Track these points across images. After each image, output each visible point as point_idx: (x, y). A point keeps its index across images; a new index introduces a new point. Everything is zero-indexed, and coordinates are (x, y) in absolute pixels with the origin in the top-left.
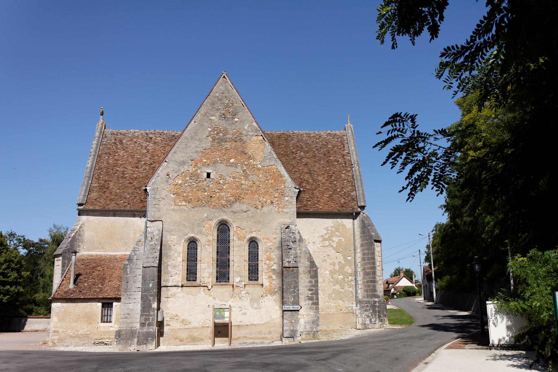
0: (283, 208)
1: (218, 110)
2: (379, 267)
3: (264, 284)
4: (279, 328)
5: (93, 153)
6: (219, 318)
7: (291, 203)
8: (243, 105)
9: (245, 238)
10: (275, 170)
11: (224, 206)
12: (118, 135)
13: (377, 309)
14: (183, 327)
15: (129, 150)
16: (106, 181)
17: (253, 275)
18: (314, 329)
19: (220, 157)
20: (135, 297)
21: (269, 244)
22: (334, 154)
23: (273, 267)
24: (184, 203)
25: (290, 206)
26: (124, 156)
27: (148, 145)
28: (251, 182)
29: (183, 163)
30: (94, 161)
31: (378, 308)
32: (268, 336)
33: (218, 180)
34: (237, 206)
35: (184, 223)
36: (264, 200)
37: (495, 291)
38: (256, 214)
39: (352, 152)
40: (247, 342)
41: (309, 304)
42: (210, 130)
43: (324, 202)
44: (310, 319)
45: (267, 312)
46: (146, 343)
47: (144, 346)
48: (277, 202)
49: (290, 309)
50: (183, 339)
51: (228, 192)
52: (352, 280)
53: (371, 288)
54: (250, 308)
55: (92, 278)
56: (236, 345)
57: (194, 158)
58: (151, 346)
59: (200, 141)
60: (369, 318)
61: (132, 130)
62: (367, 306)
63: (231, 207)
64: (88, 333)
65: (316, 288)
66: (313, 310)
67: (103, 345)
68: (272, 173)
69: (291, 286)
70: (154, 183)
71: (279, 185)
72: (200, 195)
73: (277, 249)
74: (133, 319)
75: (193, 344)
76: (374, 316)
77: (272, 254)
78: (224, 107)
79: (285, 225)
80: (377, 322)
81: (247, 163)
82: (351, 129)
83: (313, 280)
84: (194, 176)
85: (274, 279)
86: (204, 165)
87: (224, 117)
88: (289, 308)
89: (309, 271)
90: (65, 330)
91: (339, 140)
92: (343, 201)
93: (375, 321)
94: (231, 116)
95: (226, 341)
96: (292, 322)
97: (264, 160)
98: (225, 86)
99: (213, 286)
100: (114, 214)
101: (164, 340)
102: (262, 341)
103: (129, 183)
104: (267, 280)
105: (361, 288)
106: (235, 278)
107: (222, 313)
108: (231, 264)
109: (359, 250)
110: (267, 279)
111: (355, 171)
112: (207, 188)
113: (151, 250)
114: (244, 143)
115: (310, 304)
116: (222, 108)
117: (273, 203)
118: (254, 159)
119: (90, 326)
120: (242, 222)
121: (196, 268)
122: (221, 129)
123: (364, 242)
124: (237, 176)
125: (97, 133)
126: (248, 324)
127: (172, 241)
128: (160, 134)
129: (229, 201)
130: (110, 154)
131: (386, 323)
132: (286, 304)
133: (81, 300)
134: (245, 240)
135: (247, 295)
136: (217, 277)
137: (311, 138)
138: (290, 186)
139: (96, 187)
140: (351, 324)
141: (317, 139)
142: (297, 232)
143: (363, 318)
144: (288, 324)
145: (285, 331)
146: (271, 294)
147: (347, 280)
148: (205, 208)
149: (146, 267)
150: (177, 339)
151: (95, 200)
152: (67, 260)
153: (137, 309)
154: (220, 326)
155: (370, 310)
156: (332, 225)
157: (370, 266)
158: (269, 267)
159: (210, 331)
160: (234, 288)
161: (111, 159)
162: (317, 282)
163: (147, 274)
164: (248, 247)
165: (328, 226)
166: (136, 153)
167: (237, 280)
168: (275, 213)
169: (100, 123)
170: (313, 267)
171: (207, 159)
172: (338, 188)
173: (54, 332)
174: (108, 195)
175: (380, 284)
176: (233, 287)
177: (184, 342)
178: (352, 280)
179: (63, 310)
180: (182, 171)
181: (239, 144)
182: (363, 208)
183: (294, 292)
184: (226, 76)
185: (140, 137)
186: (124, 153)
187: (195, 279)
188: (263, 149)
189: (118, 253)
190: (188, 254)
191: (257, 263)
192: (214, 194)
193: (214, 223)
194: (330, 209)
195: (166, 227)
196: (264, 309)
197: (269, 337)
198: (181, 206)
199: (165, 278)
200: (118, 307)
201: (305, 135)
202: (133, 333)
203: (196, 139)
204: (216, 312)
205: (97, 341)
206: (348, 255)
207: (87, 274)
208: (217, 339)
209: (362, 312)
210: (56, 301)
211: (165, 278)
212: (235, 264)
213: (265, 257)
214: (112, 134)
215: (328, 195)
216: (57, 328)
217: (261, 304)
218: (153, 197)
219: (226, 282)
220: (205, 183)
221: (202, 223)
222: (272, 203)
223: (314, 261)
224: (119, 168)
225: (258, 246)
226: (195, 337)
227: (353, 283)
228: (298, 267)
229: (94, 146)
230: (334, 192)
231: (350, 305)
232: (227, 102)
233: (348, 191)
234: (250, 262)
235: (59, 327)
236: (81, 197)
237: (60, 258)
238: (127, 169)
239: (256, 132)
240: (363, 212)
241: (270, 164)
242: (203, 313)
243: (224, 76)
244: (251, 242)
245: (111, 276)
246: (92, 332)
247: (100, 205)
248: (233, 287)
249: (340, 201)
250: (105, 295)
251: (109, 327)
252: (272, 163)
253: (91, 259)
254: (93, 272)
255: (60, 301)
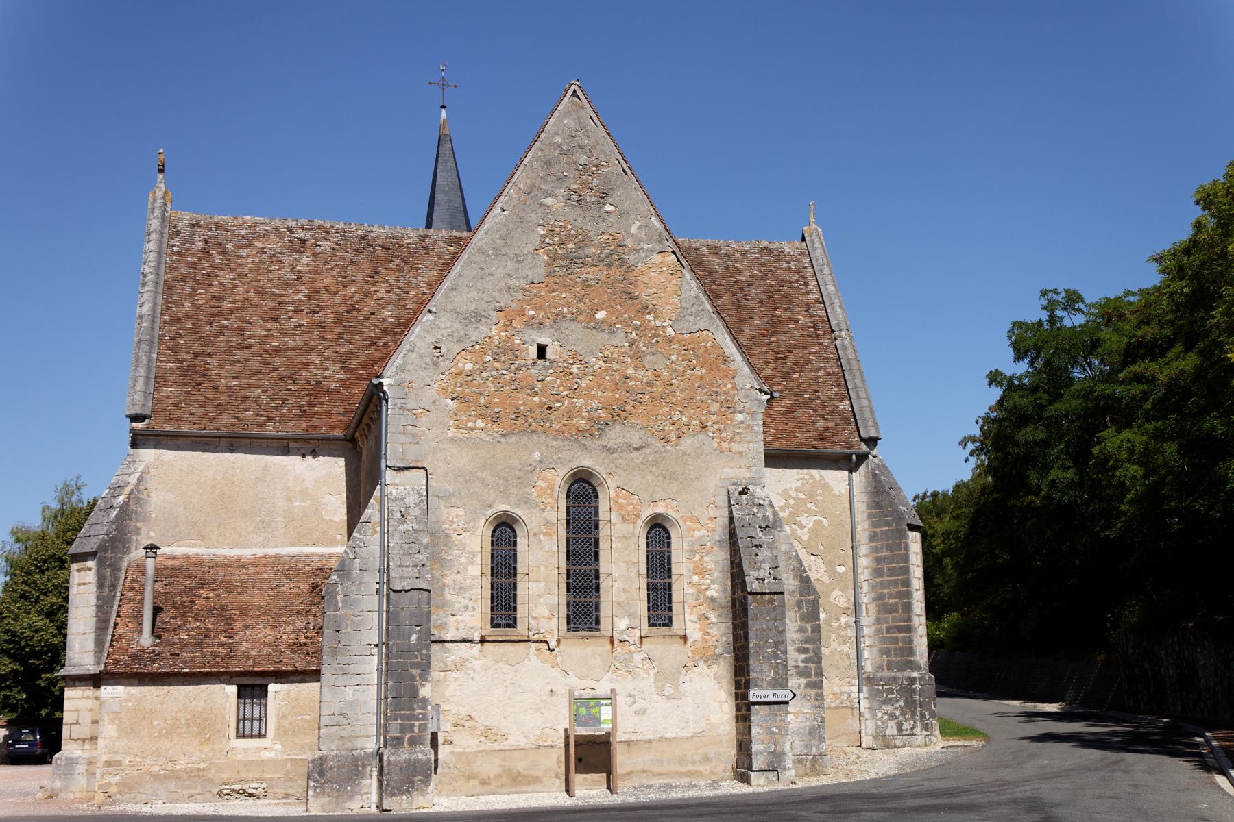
0: (732, 441)
1: (562, 180)
2: (919, 592)
3: (688, 635)
4: (727, 747)
5: (150, 277)
6: (585, 724)
7: (750, 428)
8: (624, 171)
9: (638, 516)
10: (709, 344)
11: (582, 433)
12: (210, 230)
13: (917, 697)
14: (487, 748)
15: (246, 271)
16: (196, 355)
17: (659, 612)
18: (814, 749)
19: (569, 304)
20: (360, 668)
21: (698, 534)
22: (785, 303)
23: (709, 593)
24: (480, 423)
25: (748, 437)
26: (235, 287)
27: (298, 260)
28: (649, 373)
29: (475, 318)
30: (156, 297)
31: (920, 696)
32: (702, 769)
33: (565, 365)
34: (616, 435)
35: (484, 476)
36: (684, 419)
37: (1163, 652)
38: (664, 455)
39: (830, 299)
40: (651, 783)
41: (800, 686)
42: (542, 232)
43: (775, 427)
44: (802, 724)
45: (698, 707)
46: (408, 791)
47: (404, 797)
48: (716, 426)
49: (766, 699)
50: (489, 778)
51: (592, 397)
52: (849, 626)
53: (900, 644)
54: (655, 697)
55: (195, 619)
56: (626, 794)
57: (503, 305)
58: (420, 798)
59: (519, 261)
60: (896, 721)
61: (249, 218)
62: (890, 691)
63: (600, 435)
64: (202, 766)
65: (816, 646)
66: (808, 701)
67: (242, 797)
68: (702, 351)
69: (767, 642)
70: (401, 368)
71: (720, 382)
72: (521, 402)
73: (720, 547)
74: (357, 729)
75: (514, 790)
76: (908, 716)
77: (706, 559)
78: (577, 173)
79: (738, 485)
80: (918, 730)
81: (638, 323)
82: (819, 238)
83: (809, 627)
84: (506, 352)
85: (713, 623)
86: (530, 323)
87: (576, 199)
88: (765, 696)
89: (797, 602)
90: (139, 760)
91: (792, 265)
92: (821, 423)
93: (912, 729)
94: (594, 199)
95: (599, 781)
96: (773, 733)
97: (680, 318)
98: (579, 118)
99: (563, 641)
100: (232, 445)
101: (440, 782)
102: (688, 780)
103: (261, 363)
104: (697, 626)
105: (870, 646)
106: (615, 619)
107: (594, 710)
108: (604, 583)
109: (863, 550)
110: (695, 622)
111: (844, 348)
112: (539, 386)
113: (406, 546)
114: (630, 269)
115: (802, 686)
116: (572, 176)
117: (706, 427)
118: (657, 314)
119: (206, 749)
120: (630, 476)
121: (515, 595)
122: (570, 230)
123: (878, 530)
124: (615, 356)
125: (155, 221)
126: (651, 737)
127: (452, 521)
128: (327, 232)
129: (597, 421)
130: (198, 282)
131: (935, 733)
132: (755, 686)
133: (181, 679)
134: (640, 522)
135: (647, 664)
136: (568, 616)
137: (722, 259)
138: (748, 386)
139: (172, 370)
140: (847, 735)
141: (736, 261)
142: (767, 503)
143: (878, 720)
144: (763, 737)
145: (757, 755)
146: (706, 662)
147: (836, 625)
148: (535, 437)
149: (401, 591)
150: (474, 778)
151: (176, 405)
152: (108, 570)
153: (365, 702)
154: (582, 744)
155: (897, 701)
156: (799, 484)
157: (896, 590)
158: (699, 591)
159: (555, 759)
160: (615, 645)
161: (200, 294)
162: (817, 629)
163: (402, 609)
164: (645, 541)
165: (788, 486)
166: (269, 281)
167: (622, 624)
168: (711, 453)
169: (159, 194)
170: (808, 594)
171: (537, 309)
172: (805, 391)
173: (109, 764)
174: (209, 393)
175: (921, 636)
176: (612, 642)
177: (492, 787)
178: (847, 626)
179: (130, 704)
180: (474, 338)
181: (618, 273)
182: (872, 442)
183: (776, 657)
184: (579, 92)
185: (273, 236)
186: (234, 279)
187: (511, 622)
188: (678, 289)
189: (247, 552)
190: (492, 555)
191: (666, 580)
192: (558, 401)
193: (559, 479)
194: (795, 444)
195: (434, 484)
196: (689, 699)
197: (704, 771)
198: (472, 429)
199: (437, 620)
200: (281, 696)
201: (706, 251)
202: (357, 766)
203: (506, 254)
204: (578, 707)
205: (227, 787)
206: (837, 562)
207: (176, 608)
208: (578, 779)
209: (875, 705)
210: (112, 681)
211: (437, 620)
212: (616, 585)
213: (689, 565)
214: (193, 225)
215: (783, 407)
216: (116, 753)
217: (682, 688)
218: (399, 405)
219: (590, 629)
220: (533, 371)
221: (529, 475)
222: (704, 427)
223: (808, 578)
224: (228, 319)
225: (669, 537)
226: (519, 772)
227: (851, 633)
228: (783, 593)
229: (152, 257)
230: (797, 400)
231: (845, 689)
232: (583, 160)
233: (831, 400)
234: (651, 580)
235: (121, 751)
236: (138, 397)
237: (91, 564)
238: (251, 323)
239: (660, 242)
240: (874, 453)
241: (697, 327)
242: (538, 710)
243: (575, 91)
244: (651, 529)
245: (244, 612)
246: (212, 763)
247: (192, 419)
248: (612, 642)
249: (814, 423)
250: (248, 665)
251: (259, 749)
252: (702, 325)
253: (174, 568)
254: (190, 602)
255: (122, 680)
